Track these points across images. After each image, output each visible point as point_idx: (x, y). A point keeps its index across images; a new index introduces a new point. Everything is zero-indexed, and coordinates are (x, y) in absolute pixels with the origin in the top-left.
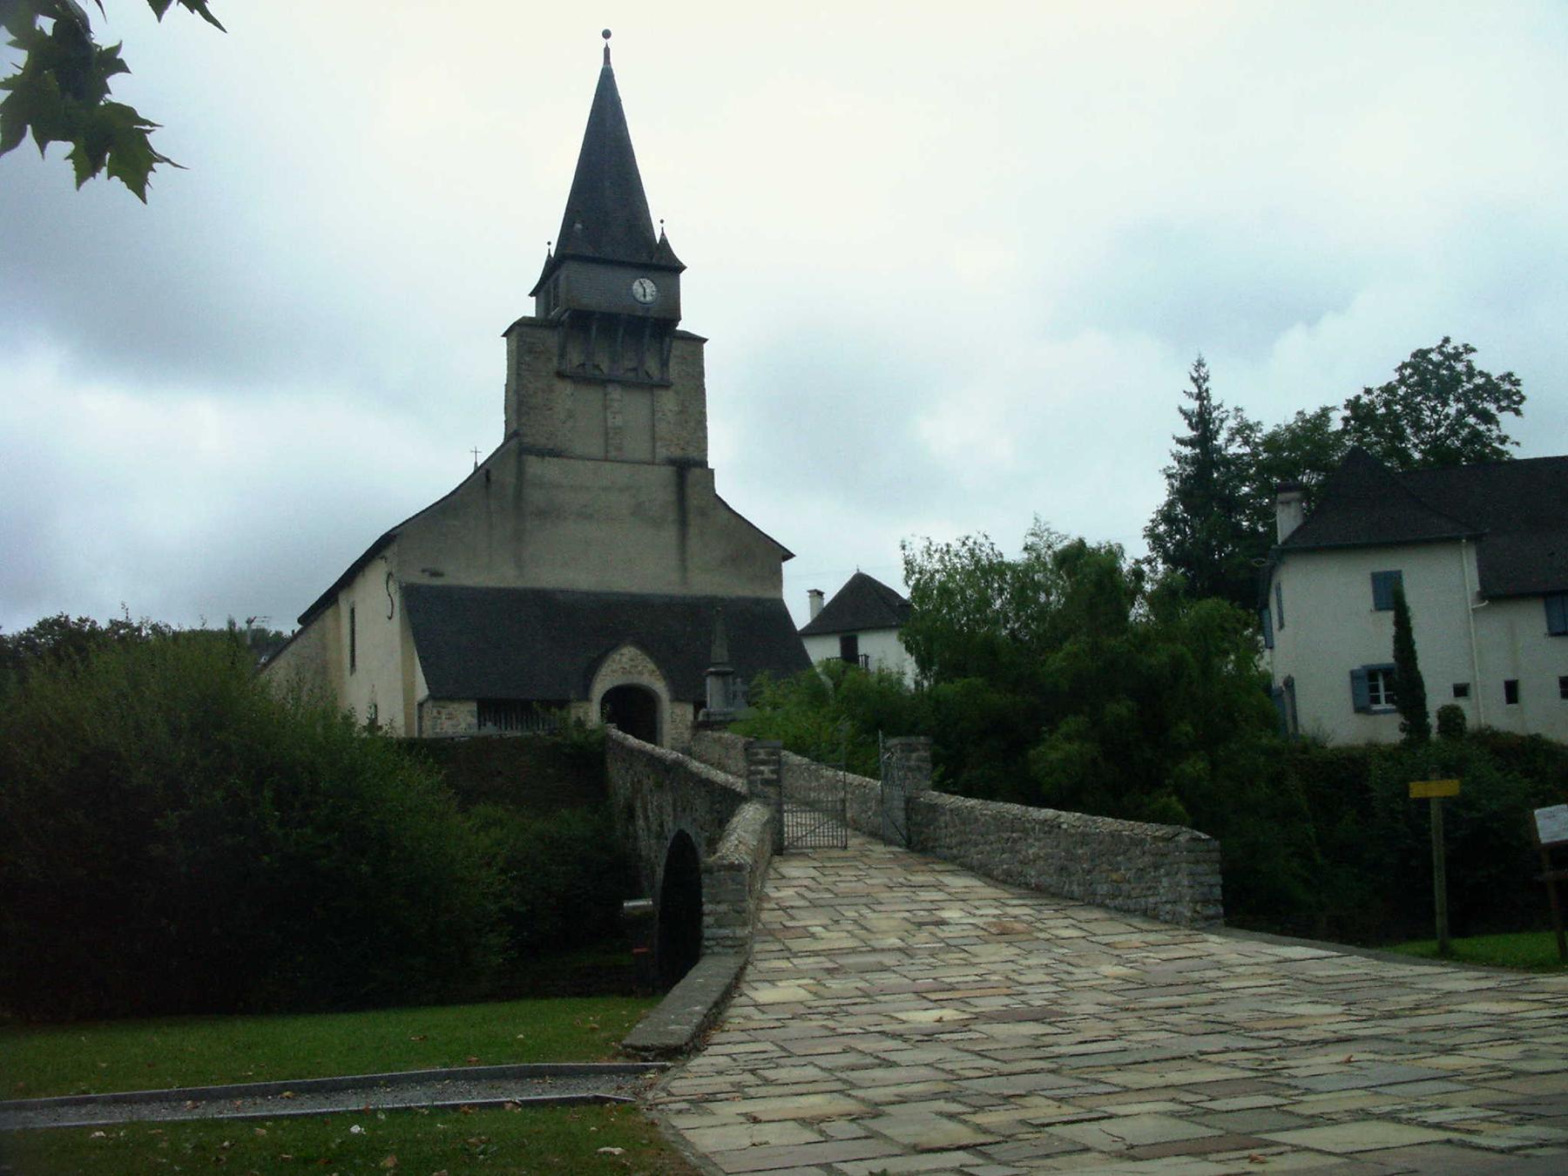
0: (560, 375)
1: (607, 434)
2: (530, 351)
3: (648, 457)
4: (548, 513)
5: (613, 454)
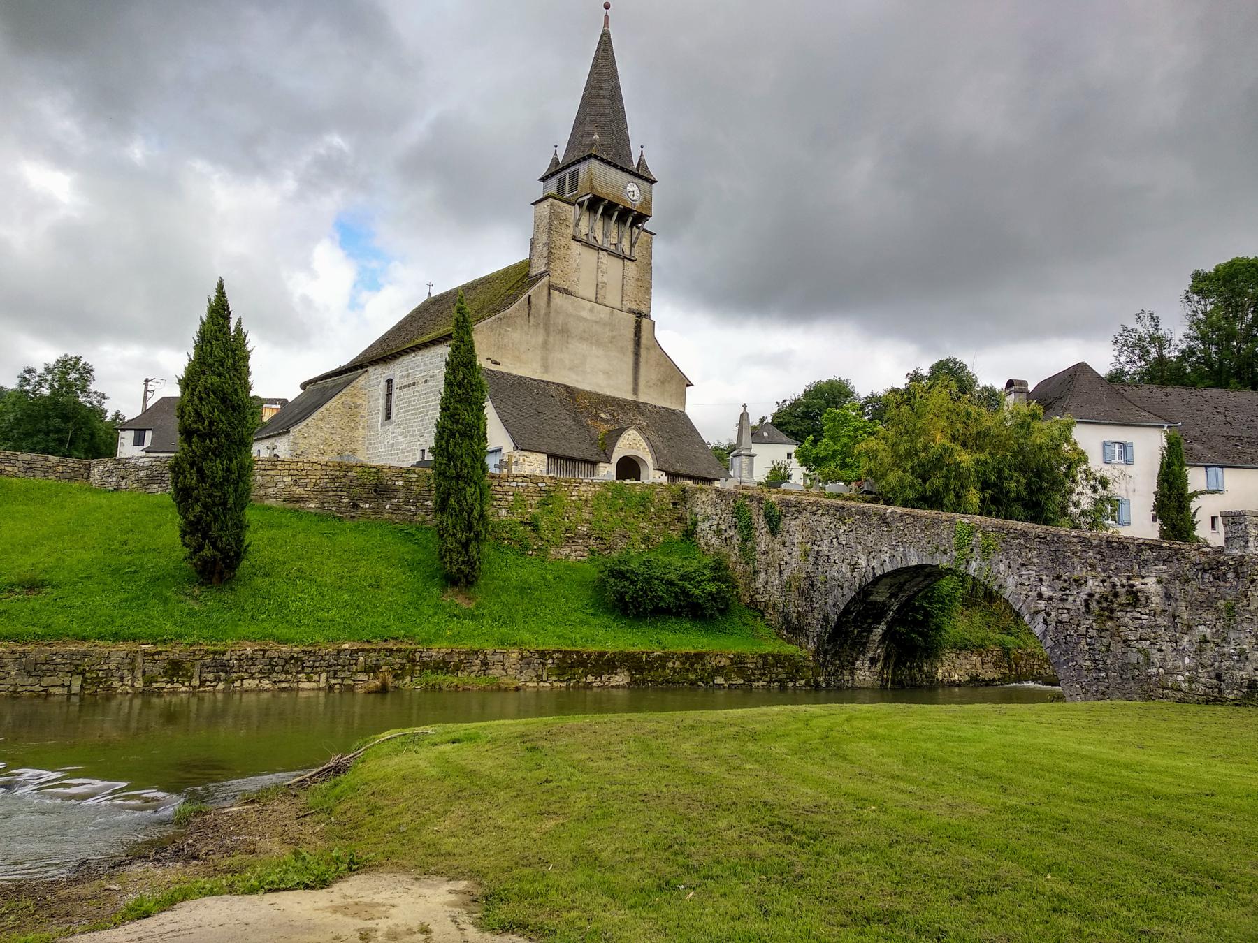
0: (575, 238)
4: (565, 332)
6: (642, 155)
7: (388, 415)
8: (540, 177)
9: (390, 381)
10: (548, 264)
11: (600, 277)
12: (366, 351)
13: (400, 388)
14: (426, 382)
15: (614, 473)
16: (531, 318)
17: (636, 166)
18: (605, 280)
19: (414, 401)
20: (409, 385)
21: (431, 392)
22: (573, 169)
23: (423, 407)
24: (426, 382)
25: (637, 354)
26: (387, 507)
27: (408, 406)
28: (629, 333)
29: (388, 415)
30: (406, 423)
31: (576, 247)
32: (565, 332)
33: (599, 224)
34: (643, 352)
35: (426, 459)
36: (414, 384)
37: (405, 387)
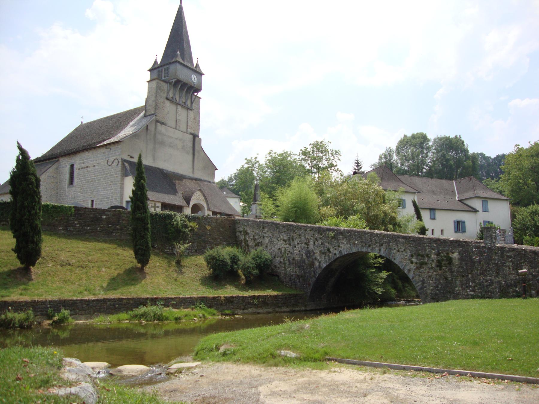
0: (167, 99)
1: (176, 121)
2: (160, 89)
3: (185, 131)
4: (162, 143)
5: (178, 128)
6: (156, 59)
7: (71, 182)
8: (148, 69)
9: (72, 166)
10: (155, 110)
12: (51, 150)
13: (79, 169)
14: (94, 166)
15: (160, 210)
16: (148, 136)
17: (195, 66)
18: (180, 118)
19: (87, 175)
20: (85, 168)
21: (97, 171)
22: (167, 66)
23: (93, 179)
24: (94, 166)
25: (194, 154)
26: (98, 229)
27: (84, 178)
28: (190, 144)
29: (71, 182)
30: (83, 187)
31: (167, 103)
33: (178, 92)
34: (196, 153)
36: (87, 167)
37: (82, 168)
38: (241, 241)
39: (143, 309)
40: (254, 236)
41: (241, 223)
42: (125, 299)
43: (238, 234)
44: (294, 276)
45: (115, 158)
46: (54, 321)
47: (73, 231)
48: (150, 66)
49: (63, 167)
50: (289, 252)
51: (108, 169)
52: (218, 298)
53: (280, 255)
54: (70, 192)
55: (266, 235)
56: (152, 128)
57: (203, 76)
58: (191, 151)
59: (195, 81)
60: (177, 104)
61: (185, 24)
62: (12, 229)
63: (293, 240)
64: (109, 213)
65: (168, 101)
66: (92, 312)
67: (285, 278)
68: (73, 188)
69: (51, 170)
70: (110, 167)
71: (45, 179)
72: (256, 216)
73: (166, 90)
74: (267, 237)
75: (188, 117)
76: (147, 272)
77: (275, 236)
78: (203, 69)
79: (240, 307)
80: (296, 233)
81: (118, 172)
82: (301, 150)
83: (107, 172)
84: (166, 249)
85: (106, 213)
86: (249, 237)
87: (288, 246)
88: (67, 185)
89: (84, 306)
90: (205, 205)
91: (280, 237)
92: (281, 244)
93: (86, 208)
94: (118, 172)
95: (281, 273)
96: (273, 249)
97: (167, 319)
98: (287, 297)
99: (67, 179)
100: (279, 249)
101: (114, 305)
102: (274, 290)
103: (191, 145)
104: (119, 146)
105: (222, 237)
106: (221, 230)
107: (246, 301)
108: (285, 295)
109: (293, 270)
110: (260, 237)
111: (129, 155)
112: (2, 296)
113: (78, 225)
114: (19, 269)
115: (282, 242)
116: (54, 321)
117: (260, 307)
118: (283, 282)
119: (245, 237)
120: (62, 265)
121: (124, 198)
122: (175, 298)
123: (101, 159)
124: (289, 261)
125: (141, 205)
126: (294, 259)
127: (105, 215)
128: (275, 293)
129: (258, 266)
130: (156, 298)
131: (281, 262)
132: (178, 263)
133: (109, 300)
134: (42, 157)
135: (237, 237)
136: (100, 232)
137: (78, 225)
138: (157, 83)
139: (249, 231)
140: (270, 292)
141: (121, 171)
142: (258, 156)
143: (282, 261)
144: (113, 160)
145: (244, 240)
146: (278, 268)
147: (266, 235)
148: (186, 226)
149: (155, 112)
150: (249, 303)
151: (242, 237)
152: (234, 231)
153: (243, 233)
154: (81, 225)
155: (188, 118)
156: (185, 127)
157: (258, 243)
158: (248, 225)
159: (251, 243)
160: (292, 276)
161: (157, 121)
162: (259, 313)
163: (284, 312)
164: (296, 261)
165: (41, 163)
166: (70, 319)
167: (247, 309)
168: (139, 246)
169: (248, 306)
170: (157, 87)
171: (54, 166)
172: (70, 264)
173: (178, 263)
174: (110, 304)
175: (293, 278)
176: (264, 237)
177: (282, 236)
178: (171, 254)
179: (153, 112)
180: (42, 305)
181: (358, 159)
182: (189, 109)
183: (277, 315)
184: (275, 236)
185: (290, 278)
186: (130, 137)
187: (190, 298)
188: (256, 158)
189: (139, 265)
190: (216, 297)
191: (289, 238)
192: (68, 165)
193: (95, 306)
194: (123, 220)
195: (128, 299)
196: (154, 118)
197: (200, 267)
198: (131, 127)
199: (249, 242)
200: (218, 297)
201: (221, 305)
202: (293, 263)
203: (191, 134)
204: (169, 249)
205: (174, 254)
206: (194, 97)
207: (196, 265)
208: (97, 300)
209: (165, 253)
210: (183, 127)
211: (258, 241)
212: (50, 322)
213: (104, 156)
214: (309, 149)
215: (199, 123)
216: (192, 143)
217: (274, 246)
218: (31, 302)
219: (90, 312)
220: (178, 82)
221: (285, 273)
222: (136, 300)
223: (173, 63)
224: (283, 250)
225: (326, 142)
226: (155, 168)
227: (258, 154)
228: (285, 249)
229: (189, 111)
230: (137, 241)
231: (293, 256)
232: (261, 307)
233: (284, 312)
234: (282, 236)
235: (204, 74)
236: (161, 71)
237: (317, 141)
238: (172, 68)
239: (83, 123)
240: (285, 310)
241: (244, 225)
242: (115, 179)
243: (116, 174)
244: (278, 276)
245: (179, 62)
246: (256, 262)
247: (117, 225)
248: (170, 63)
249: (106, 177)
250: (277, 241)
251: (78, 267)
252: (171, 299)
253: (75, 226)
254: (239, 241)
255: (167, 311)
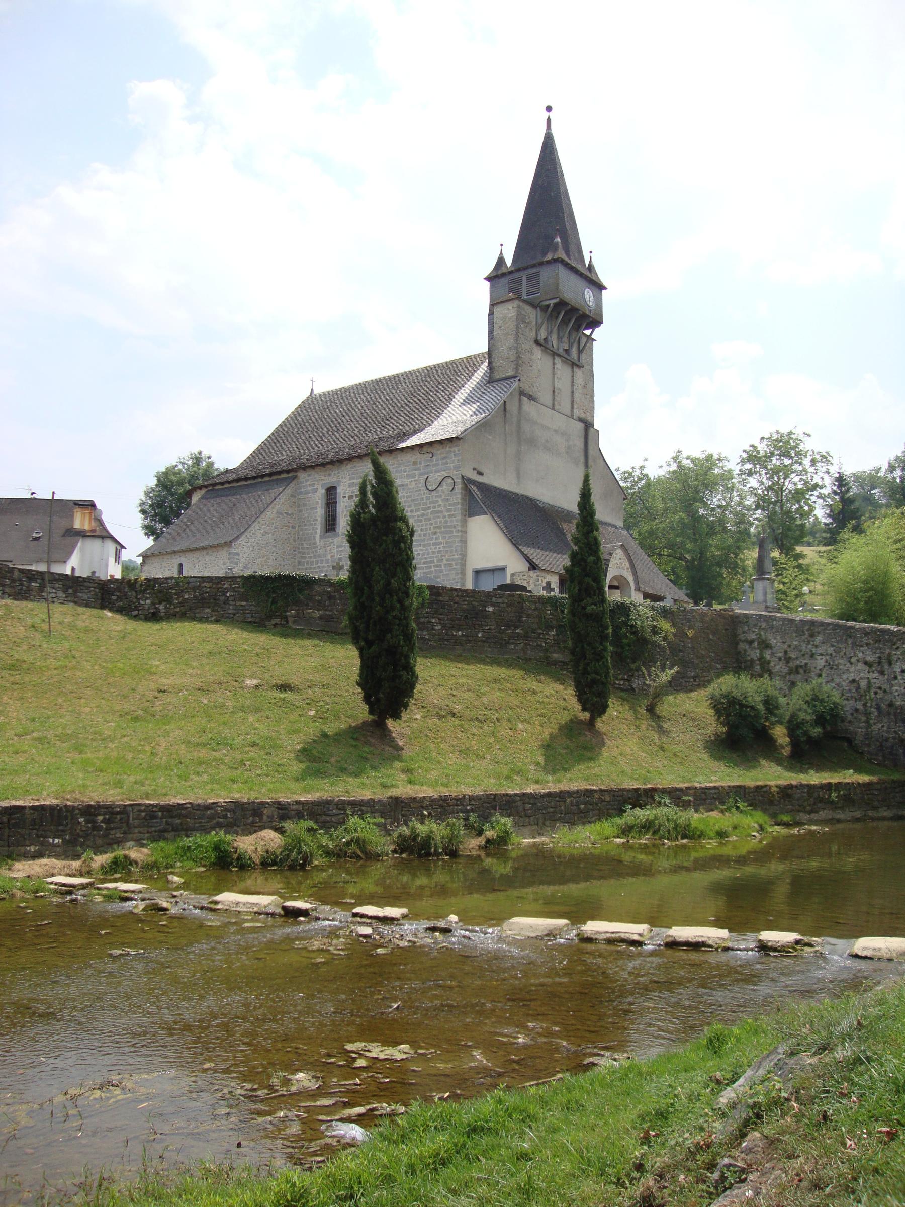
0: (537, 342)
1: (554, 392)
2: (524, 322)
5: (556, 407)
6: (501, 253)
8: (486, 275)
10: (517, 369)
11: (556, 384)
22: (534, 270)
31: (538, 352)
32: (532, 442)
35: (185, 574)
38: (752, 661)
39: (643, 814)
40: (786, 652)
41: (751, 622)
42: (595, 791)
43: (742, 646)
44: (891, 740)
45: (445, 474)
46: (488, 841)
47: (429, 640)
48: (489, 267)
49: (308, 493)
50: (880, 688)
51: (428, 498)
52: (764, 789)
53: (855, 695)
54: (328, 549)
55: (820, 651)
56: (513, 408)
57: (604, 291)
58: (582, 459)
59: (591, 304)
60: (554, 354)
61: (562, 174)
62: (356, 640)
63: (890, 664)
64: (500, 600)
65: (539, 347)
66: (541, 821)
67: (869, 745)
68: (336, 540)
69: (283, 498)
70: (434, 494)
71: (273, 519)
72: (767, 607)
73: (534, 323)
74: (822, 655)
75: (573, 382)
76: (604, 730)
77: (842, 654)
78: (604, 279)
79: (805, 807)
80: (897, 648)
81: (454, 505)
82: (744, 451)
83: (424, 504)
84: (617, 679)
85: (494, 600)
86: (773, 654)
87: (876, 675)
88: (319, 531)
89: (528, 806)
90: (630, 579)
91: (855, 655)
92: (858, 672)
93: (452, 590)
94: (454, 505)
95: (856, 733)
96: (837, 680)
97: (702, 835)
98: (889, 785)
99: (319, 519)
100: (854, 681)
101: (578, 805)
102: (859, 770)
103: (582, 446)
104: (456, 449)
105: (714, 652)
106: (711, 637)
107: (815, 795)
108: (885, 782)
109: (889, 728)
110: (804, 655)
111: (474, 469)
112: (899, 818)
113: (438, 627)
114: (365, 723)
115: (860, 666)
116: (488, 841)
117: (840, 808)
118: (862, 753)
119: (761, 654)
120: (440, 717)
121: (468, 563)
122: (688, 788)
123: (408, 476)
124: (878, 708)
125: (594, 585)
126: (891, 705)
127: (493, 605)
128: (864, 778)
129: (820, 720)
130: (654, 790)
131: (857, 710)
132: (651, 709)
133: (570, 793)
134: (243, 465)
135: (740, 652)
136: (484, 642)
137: (438, 627)
138: (519, 307)
139: (773, 642)
140: (849, 776)
141: (462, 505)
142: (646, 464)
143: (859, 706)
144: (440, 479)
145: (759, 660)
146: (850, 722)
147: (820, 651)
148: (655, 630)
149: (517, 372)
150: (821, 800)
151: (754, 654)
152: (734, 640)
153: (755, 644)
154: (444, 626)
155: (573, 386)
156: (569, 407)
157: (797, 667)
158: (772, 627)
159: (778, 667)
160: (887, 740)
161: (522, 393)
162: (839, 821)
163: (884, 819)
164: (897, 708)
165: (249, 482)
166: (514, 839)
167: (817, 812)
168: (594, 675)
169: (819, 805)
170: (518, 315)
171: (289, 491)
172: (454, 715)
173: (651, 709)
174: (571, 802)
175: (889, 744)
176: (812, 656)
177: (860, 655)
178: (627, 690)
179: (511, 373)
180: (457, 805)
181: (842, 470)
182: (575, 365)
183: (871, 824)
184: (842, 654)
185: (881, 746)
186: (476, 428)
187: (715, 788)
188: (642, 468)
189: (587, 715)
190: (762, 787)
191: (880, 658)
192: (320, 487)
193: (545, 808)
194: (528, 616)
195: (601, 790)
196: (516, 385)
197: (693, 720)
198: (462, 405)
199: (772, 664)
200: (766, 786)
201: (771, 802)
202: (889, 714)
203: (581, 420)
204: (623, 679)
205: (633, 690)
206: (584, 340)
207: (684, 715)
208: (550, 794)
209: (617, 688)
210: (565, 406)
211: (798, 663)
212: (481, 841)
213: (418, 469)
214: (762, 448)
215: (592, 396)
216: (583, 440)
217: (840, 676)
218: (439, 800)
219: (538, 819)
220: (562, 303)
221: (867, 734)
222: (616, 793)
223: (549, 262)
224: (863, 684)
225: (799, 432)
226: (523, 496)
227: (646, 460)
228: (869, 682)
229: (576, 369)
230: (588, 664)
231: (888, 697)
232: (842, 808)
233: (884, 819)
234: (860, 655)
235: (605, 288)
236: (519, 281)
237: (778, 432)
238: (546, 274)
239: (315, 392)
240: (885, 814)
241: (760, 628)
242: (446, 522)
243: (449, 511)
244: (849, 741)
245: (562, 261)
246: (815, 711)
247: (517, 627)
248: (541, 264)
249: (423, 515)
250: (848, 665)
251: (471, 720)
252: (680, 790)
253: (433, 629)
254: (746, 662)
255: (695, 818)
